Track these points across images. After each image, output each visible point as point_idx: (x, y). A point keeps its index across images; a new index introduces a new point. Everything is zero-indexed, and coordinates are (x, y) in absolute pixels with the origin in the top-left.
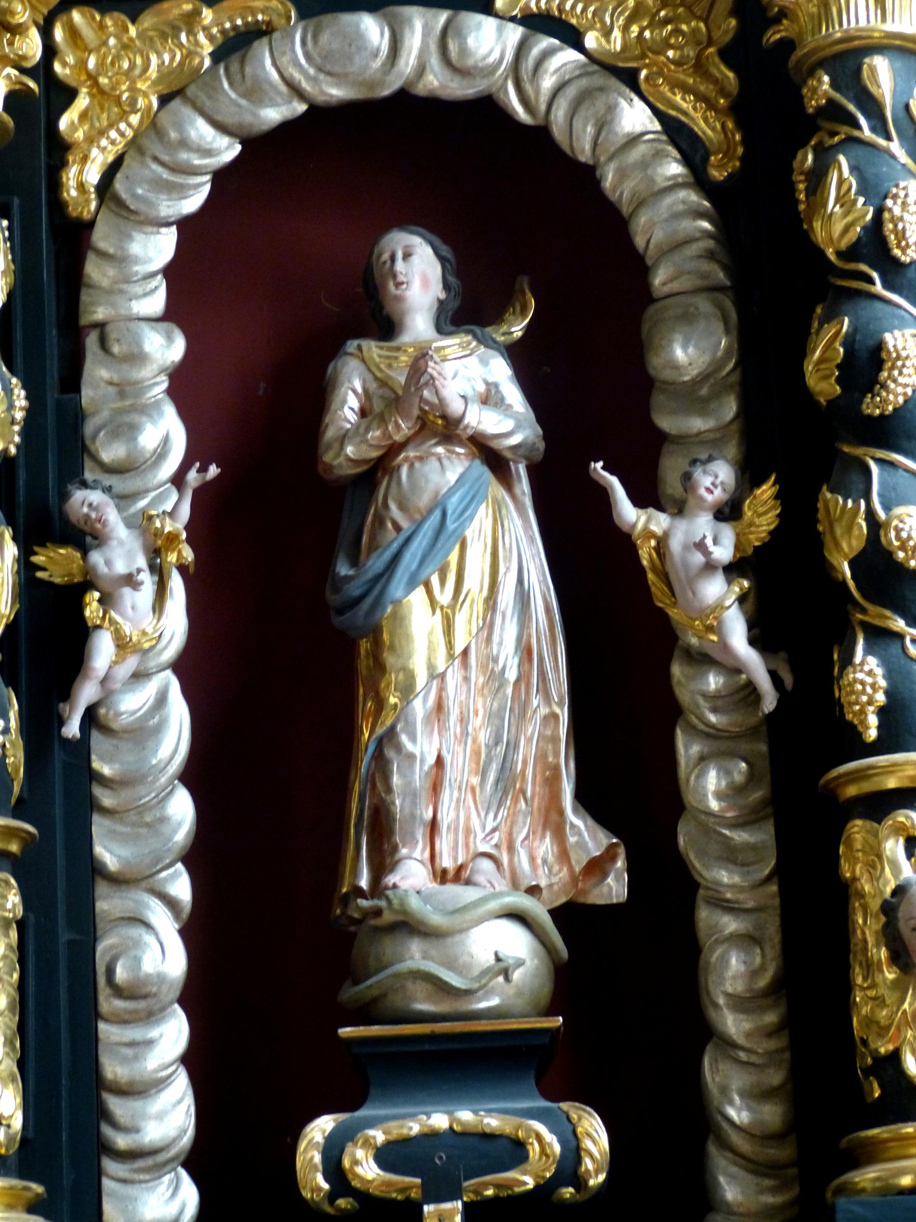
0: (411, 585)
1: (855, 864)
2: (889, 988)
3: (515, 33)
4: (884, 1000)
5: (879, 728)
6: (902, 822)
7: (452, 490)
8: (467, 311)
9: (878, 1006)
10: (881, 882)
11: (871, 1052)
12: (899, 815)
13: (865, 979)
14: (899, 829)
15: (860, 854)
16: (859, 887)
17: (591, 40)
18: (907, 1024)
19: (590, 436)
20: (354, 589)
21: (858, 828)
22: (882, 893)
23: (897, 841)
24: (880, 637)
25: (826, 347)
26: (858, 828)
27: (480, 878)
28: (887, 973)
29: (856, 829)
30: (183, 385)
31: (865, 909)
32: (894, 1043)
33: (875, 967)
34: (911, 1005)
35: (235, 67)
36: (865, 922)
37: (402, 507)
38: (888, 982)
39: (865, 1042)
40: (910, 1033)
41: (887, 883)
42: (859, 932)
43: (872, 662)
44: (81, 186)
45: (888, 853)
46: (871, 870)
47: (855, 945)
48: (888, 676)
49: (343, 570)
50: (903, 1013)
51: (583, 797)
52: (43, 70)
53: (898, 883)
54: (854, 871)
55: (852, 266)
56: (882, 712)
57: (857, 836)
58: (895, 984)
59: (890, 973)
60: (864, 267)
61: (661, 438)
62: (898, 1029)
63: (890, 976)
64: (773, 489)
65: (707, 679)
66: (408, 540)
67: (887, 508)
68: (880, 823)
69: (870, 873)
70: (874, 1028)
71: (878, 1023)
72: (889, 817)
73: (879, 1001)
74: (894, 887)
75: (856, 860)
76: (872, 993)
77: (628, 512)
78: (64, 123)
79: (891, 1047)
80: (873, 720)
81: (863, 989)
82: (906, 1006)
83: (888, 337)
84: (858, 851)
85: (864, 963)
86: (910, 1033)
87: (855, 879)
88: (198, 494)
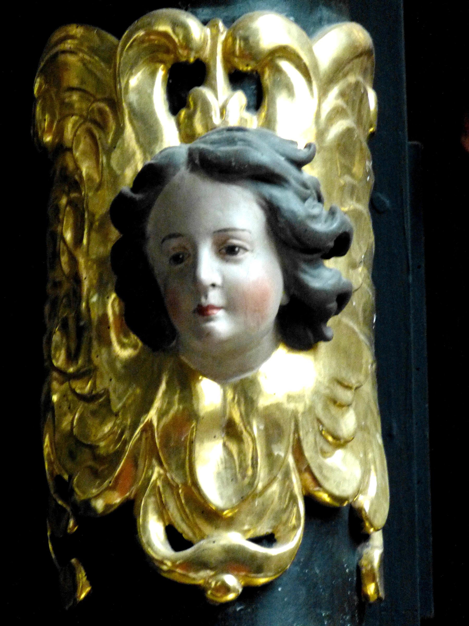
1: (64, 118)
2: (119, 378)
4: (108, 401)
6: (165, 35)
9: (94, 413)
10: (115, 155)
11: (75, 507)
12: (159, 20)
13: (72, 357)
14: (157, 50)
15: (75, 97)
16: (71, 165)
18: (153, 452)
22: (116, 179)
23: (153, 74)
28: (117, 348)
29: (69, 44)
31: (78, 208)
32: (122, 493)
33: (94, 334)
34: (162, 414)
36: (78, 240)
38: (119, 365)
39: (65, 489)
40: (157, 470)
41: (127, 159)
42: (64, 259)
45: (133, 97)
46: (96, 132)
47: (57, 285)
49: (156, 42)
50: (144, 430)
53: (149, 161)
54: (60, 132)
57: (72, 59)
58: (132, 370)
59: (123, 346)
62: (134, 461)
63: (123, 351)
65: (160, 66)
68: (119, 37)
69: (93, 136)
70: (85, 457)
71: (93, 448)
72: (138, 23)
73: (98, 404)
74: (140, 167)
75: (67, 109)
76: (85, 387)
79: (117, 499)
81: (66, 377)
82: (152, 415)
84: (72, 89)
85: (71, 323)
86: (157, 470)
87: (61, 149)
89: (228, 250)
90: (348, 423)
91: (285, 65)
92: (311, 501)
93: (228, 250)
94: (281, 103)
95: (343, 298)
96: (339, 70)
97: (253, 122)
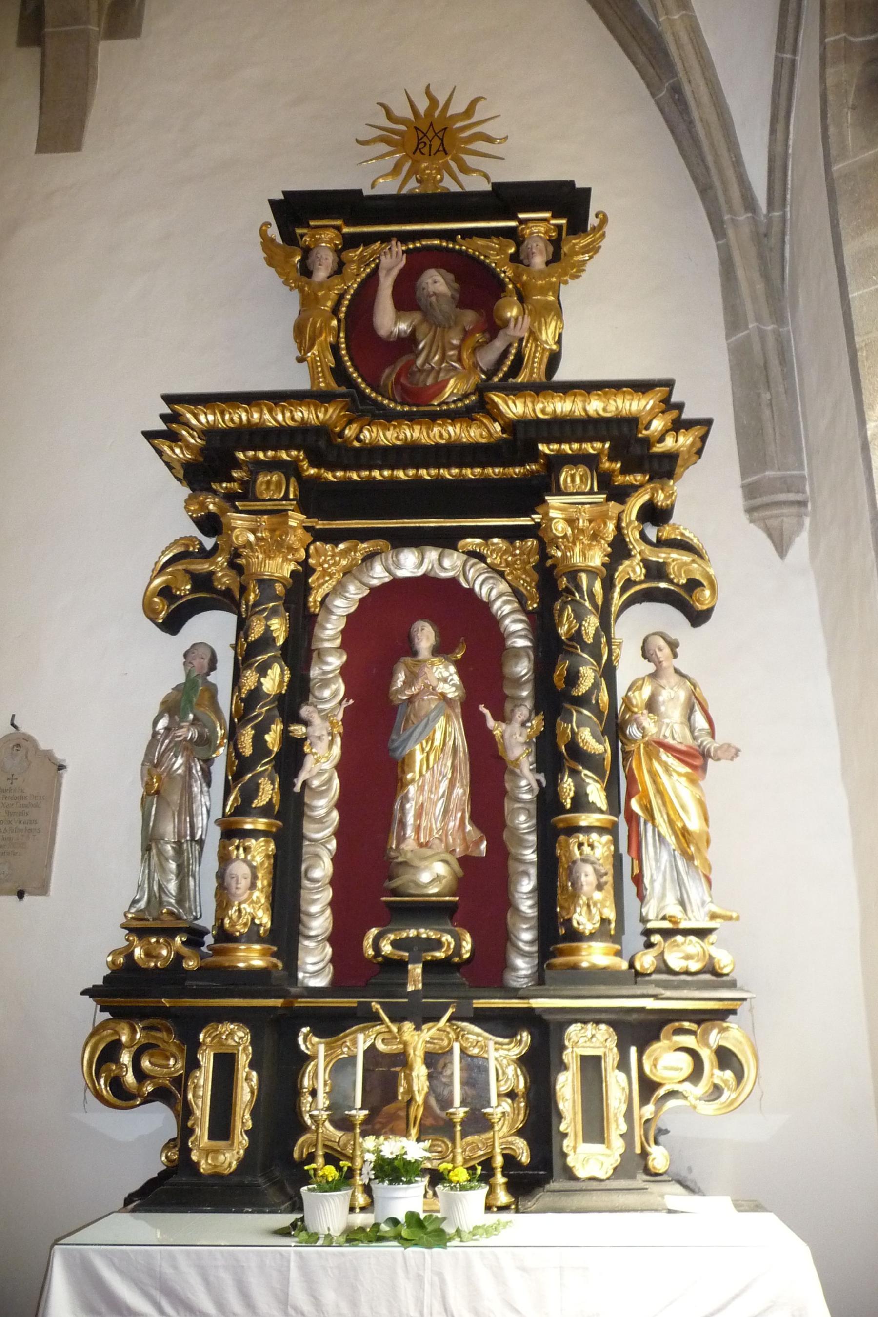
0: (416, 743)
3: (465, 557)
5: (571, 804)
7: (432, 711)
8: (441, 650)
17: (489, 561)
19: (484, 687)
20: (396, 744)
21: (562, 838)
24: (574, 773)
25: (562, 668)
26: (562, 838)
27: (434, 847)
30: (345, 671)
35: (369, 564)
37: (415, 715)
43: (570, 780)
44: (315, 602)
48: (575, 786)
51: (472, 818)
52: (305, 563)
55: (571, 643)
56: (572, 799)
60: (575, 644)
61: (506, 697)
64: (158, 1269)
66: (416, 728)
67: (578, 727)
77: (491, 723)
78: (310, 581)
80: (569, 801)
83: (581, 668)
88: (346, 709)
89: (660, 650)
90: (608, 904)
91: (411, 884)
92: (602, 918)
93: (586, 875)
94: (596, 850)
95: (606, 883)
96: (606, 844)
97: (592, 853)
